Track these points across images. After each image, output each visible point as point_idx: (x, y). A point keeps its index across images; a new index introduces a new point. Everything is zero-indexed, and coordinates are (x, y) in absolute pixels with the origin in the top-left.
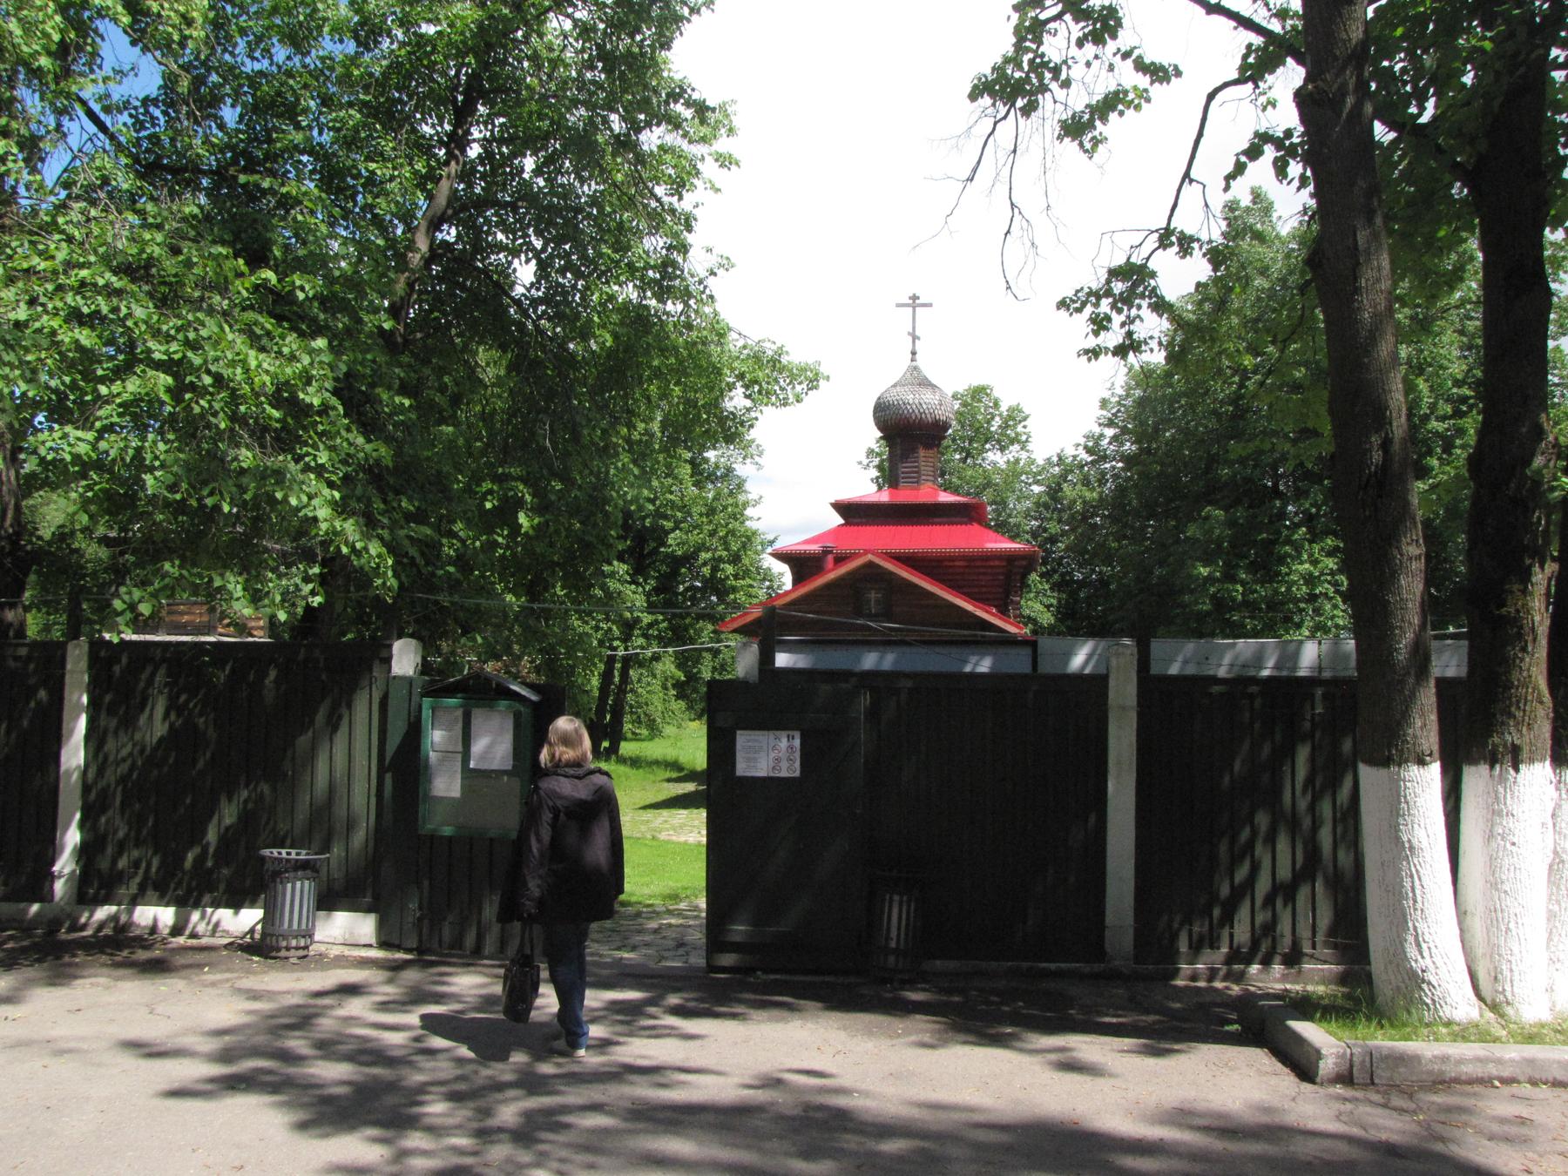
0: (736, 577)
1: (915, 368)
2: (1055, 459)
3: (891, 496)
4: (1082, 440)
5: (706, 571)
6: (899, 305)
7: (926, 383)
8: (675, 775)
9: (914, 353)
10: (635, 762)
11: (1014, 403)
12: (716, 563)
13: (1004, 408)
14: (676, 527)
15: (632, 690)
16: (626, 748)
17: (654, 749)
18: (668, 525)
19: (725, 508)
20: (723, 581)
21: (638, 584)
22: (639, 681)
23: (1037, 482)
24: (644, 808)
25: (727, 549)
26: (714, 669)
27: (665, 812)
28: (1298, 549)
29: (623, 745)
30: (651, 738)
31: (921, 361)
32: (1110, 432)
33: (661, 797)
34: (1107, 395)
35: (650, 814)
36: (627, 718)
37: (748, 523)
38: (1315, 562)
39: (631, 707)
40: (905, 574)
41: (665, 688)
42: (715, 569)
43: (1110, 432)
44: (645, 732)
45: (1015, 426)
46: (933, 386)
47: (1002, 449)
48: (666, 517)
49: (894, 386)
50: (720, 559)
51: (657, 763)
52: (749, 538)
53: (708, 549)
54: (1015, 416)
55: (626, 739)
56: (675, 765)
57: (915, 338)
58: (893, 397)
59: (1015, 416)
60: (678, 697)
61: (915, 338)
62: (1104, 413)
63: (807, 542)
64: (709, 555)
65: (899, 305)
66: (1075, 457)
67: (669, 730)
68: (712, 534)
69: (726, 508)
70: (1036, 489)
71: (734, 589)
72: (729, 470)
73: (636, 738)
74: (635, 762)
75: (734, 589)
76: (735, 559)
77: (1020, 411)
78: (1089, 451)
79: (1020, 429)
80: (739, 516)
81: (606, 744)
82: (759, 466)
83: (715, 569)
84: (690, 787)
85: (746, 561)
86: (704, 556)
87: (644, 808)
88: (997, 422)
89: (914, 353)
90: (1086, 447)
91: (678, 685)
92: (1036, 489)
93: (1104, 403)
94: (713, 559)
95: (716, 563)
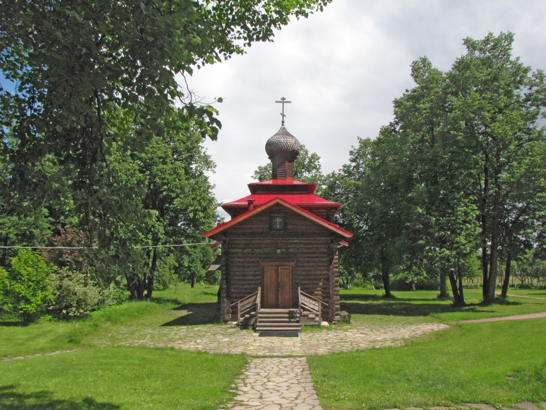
0: (204, 218)
1: (284, 128)
2: (331, 175)
3: (273, 182)
4: (342, 168)
5: (191, 215)
6: (276, 102)
7: (288, 134)
8: (177, 306)
9: (283, 122)
10: (158, 300)
11: (313, 152)
12: (195, 211)
13: (310, 155)
14: (177, 196)
15: (157, 270)
16: (155, 294)
17: (166, 294)
18: (174, 195)
19: (200, 187)
20: (198, 219)
21: (161, 222)
22: (160, 266)
23: (324, 184)
24: (165, 325)
25: (201, 206)
26: (189, 262)
27: (175, 328)
28: (459, 200)
29: (153, 292)
30: (164, 289)
31: (286, 126)
32: (354, 164)
33: (171, 319)
34: (352, 150)
35: (167, 329)
36: (155, 281)
37: (209, 195)
38: (466, 206)
39: (157, 277)
40: (295, 209)
41: (170, 269)
42: (195, 214)
43: (354, 164)
44: (161, 287)
45: (315, 161)
46: (292, 136)
47: (309, 171)
48: (173, 192)
49: (275, 135)
50: (197, 210)
51: (168, 301)
52: (211, 200)
53: (192, 206)
54: (315, 157)
55: (154, 290)
56: (175, 302)
57: (283, 116)
58: (275, 140)
59: (315, 157)
60: (175, 273)
61: (283, 116)
62: (352, 157)
63: (237, 201)
64: (193, 208)
65: (276, 102)
66: (339, 174)
67: (171, 286)
68: (194, 199)
69: (201, 188)
70: (324, 187)
71: (203, 224)
72: (201, 173)
73: (158, 290)
74: (158, 300)
75: (203, 224)
76: (204, 210)
77: (317, 155)
78: (345, 172)
79: (316, 163)
80: (206, 191)
81: (145, 292)
82: (214, 172)
83: (195, 214)
84: (184, 313)
85: (209, 211)
86: (191, 208)
87: (165, 325)
88: (307, 160)
89: (283, 122)
90: (343, 170)
91: (175, 268)
92: (324, 187)
93: (351, 153)
94: (194, 209)
95: (195, 211)
